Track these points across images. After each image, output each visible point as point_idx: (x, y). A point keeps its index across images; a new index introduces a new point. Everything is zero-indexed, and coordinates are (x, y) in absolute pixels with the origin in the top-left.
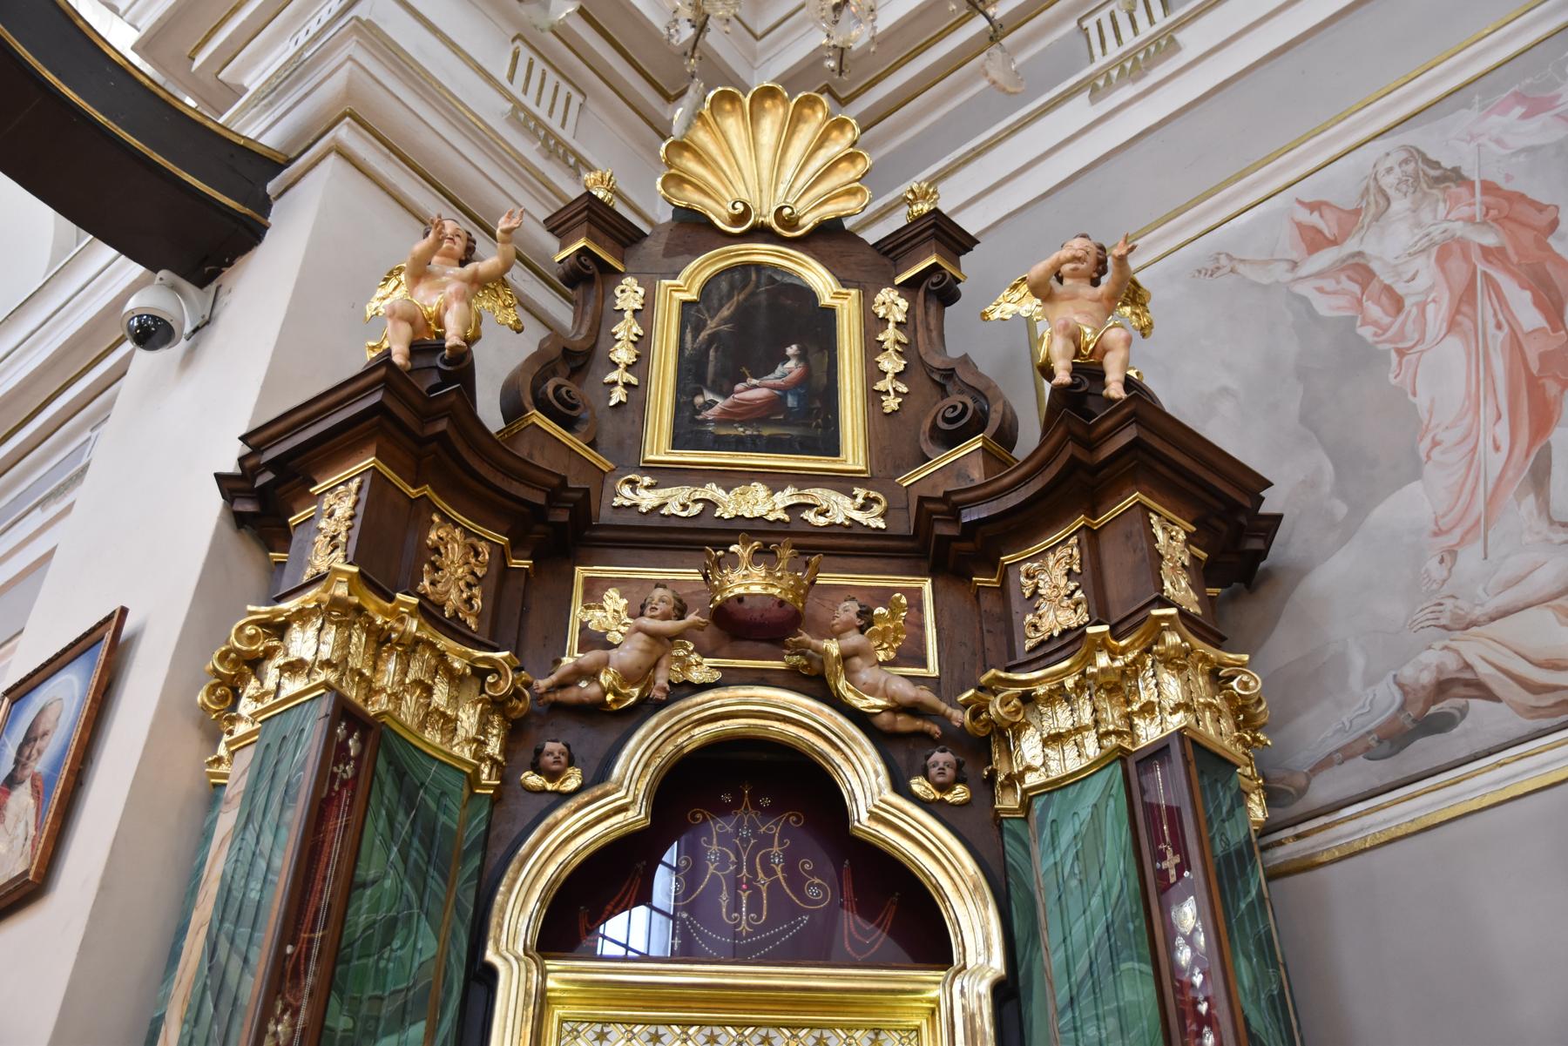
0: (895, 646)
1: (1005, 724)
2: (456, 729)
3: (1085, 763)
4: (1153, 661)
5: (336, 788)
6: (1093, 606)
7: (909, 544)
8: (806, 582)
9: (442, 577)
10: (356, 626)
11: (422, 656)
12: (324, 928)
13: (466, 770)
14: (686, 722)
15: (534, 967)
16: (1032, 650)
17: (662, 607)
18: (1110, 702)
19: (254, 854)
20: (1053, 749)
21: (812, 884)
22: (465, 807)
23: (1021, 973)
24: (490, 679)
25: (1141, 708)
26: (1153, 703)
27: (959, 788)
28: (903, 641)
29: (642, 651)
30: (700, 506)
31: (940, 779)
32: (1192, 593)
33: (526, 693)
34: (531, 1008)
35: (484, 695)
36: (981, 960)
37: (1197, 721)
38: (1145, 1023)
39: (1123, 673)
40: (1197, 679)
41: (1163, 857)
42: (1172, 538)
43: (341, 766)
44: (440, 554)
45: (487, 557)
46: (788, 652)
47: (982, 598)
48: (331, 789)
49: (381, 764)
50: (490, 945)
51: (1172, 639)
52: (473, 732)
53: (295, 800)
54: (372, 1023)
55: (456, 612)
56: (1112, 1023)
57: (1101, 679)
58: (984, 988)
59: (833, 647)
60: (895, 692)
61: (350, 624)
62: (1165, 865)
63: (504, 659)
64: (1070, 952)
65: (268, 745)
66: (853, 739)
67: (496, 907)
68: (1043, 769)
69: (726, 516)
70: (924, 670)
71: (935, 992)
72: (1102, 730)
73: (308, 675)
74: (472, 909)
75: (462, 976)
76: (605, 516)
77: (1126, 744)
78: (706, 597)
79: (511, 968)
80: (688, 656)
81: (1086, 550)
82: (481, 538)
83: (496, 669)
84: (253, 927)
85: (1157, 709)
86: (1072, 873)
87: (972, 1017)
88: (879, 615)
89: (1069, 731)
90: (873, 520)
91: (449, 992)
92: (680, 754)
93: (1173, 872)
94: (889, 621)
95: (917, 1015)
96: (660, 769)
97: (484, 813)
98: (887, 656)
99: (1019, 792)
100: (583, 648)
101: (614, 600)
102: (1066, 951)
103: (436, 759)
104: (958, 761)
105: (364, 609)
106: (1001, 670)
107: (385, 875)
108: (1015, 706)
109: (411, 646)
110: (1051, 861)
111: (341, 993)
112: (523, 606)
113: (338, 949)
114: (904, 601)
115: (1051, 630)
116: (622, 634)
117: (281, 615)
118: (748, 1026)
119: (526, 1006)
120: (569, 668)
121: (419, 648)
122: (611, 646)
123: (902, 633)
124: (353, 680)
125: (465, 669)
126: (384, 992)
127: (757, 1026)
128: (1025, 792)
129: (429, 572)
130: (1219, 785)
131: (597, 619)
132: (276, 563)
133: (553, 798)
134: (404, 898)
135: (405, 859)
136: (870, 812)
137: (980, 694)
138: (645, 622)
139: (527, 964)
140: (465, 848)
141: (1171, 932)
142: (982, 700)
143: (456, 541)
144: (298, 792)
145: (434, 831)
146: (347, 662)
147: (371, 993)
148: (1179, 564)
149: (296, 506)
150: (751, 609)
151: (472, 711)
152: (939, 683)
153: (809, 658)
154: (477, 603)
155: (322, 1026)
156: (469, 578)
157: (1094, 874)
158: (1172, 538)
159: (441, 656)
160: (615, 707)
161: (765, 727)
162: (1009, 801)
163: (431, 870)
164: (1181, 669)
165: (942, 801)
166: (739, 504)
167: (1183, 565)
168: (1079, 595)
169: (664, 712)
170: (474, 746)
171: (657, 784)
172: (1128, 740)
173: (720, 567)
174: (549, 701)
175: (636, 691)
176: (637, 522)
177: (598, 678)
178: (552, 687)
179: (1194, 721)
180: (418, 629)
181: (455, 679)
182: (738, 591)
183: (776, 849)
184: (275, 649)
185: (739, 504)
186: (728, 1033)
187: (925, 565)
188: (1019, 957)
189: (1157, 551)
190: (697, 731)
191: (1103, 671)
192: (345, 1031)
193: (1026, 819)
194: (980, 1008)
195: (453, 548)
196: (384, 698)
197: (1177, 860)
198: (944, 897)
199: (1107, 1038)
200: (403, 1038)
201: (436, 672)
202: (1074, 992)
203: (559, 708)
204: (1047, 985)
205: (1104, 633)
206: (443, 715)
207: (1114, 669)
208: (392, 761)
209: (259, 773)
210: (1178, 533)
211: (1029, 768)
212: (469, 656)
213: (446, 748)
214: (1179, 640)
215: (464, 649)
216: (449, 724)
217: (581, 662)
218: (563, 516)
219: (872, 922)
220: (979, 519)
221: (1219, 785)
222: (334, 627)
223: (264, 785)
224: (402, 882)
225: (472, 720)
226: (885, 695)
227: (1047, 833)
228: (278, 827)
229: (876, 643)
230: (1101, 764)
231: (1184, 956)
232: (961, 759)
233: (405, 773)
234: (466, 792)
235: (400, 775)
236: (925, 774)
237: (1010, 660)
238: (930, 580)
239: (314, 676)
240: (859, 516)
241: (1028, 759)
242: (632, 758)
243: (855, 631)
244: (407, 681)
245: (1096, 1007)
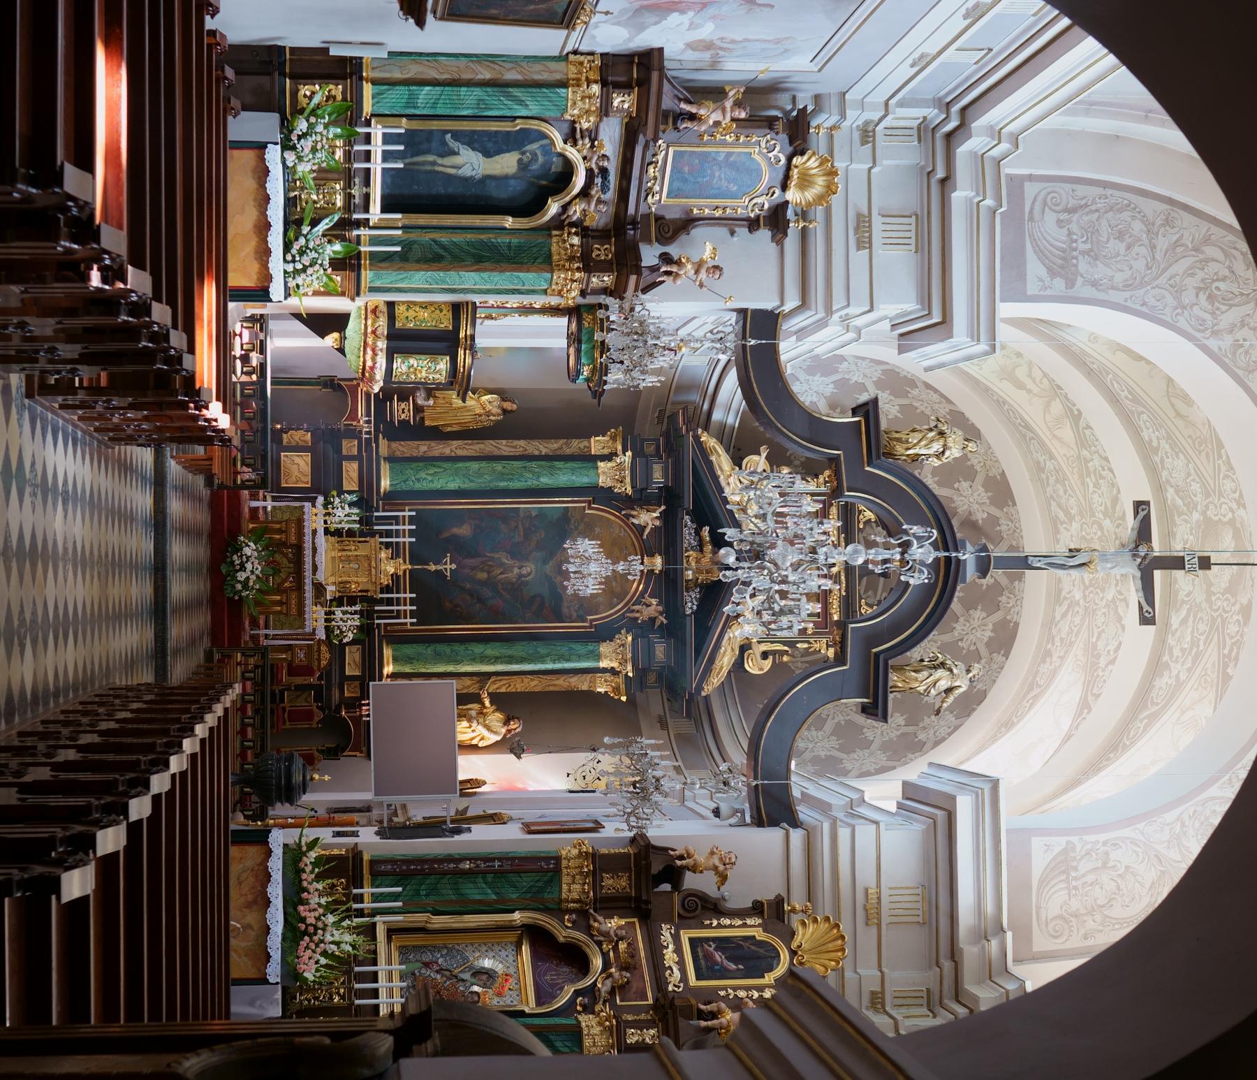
235: (550, 881)
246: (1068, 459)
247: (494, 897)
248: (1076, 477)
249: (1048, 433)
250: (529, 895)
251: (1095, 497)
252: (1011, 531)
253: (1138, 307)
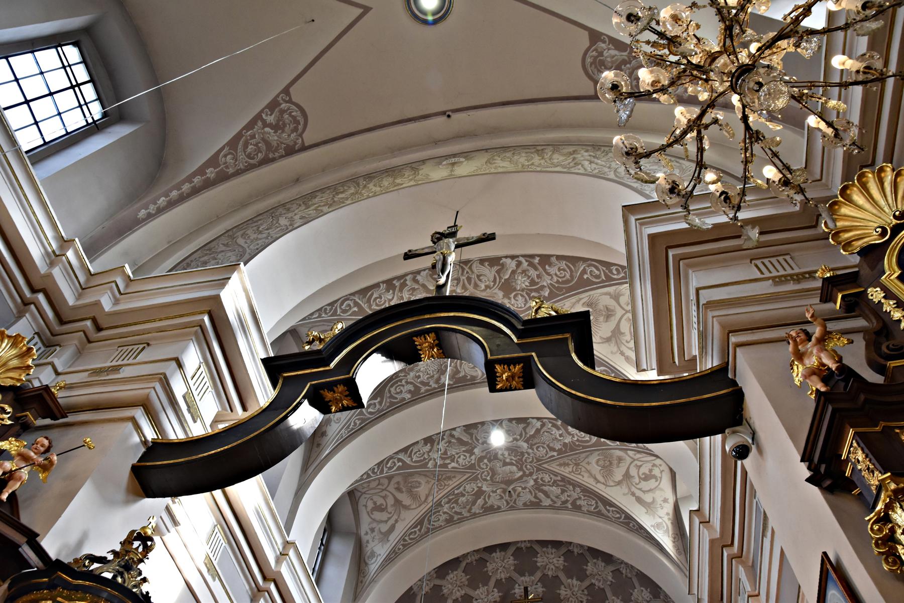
246: (440, 489)
248: (451, 482)
249: (423, 506)
251: (461, 460)
252: (504, 570)
253: (257, 251)
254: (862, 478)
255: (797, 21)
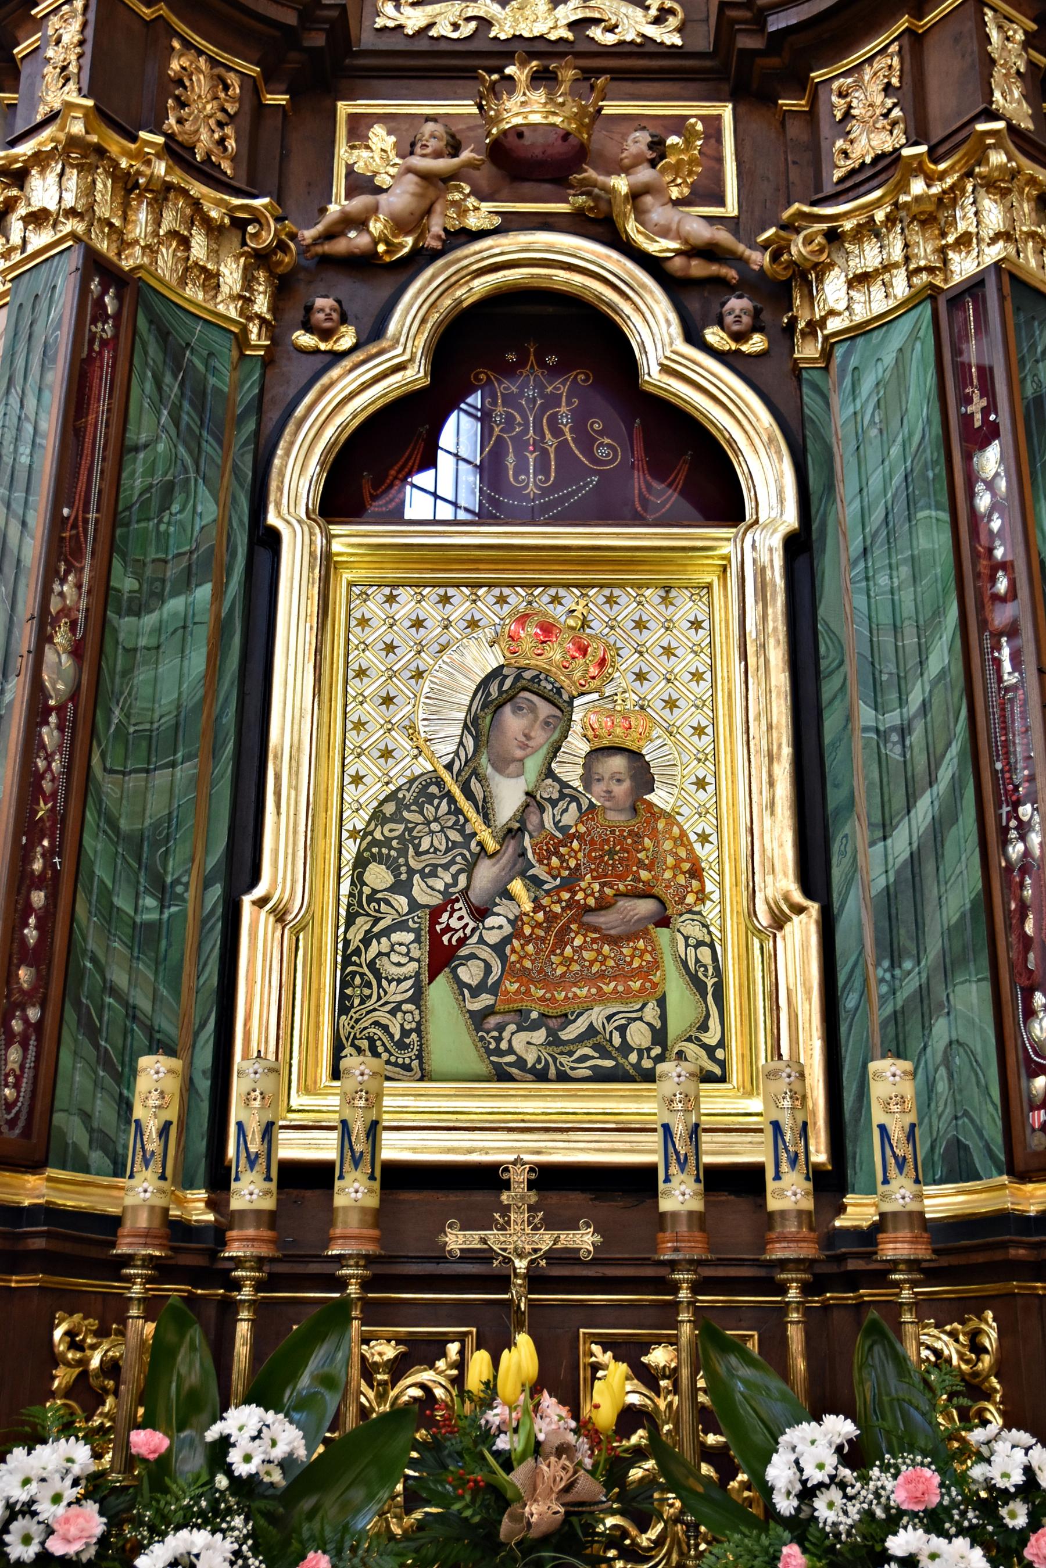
0: (689, 180)
1: (808, 265)
2: (219, 286)
3: (892, 303)
4: (974, 186)
5: (96, 347)
6: (911, 124)
7: (708, 63)
8: (591, 109)
9: (190, 114)
10: (100, 171)
11: (175, 204)
12: (98, 511)
13: (233, 329)
14: (464, 272)
15: (317, 531)
16: (841, 180)
17: (433, 144)
18: (923, 235)
19: (19, 418)
20: (859, 291)
21: (601, 444)
22: (235, 369)
23: (815, 527)
24: (251, 229)
25: (957, 239)
26: (970, 233)
27: (757, 337)
28: (698, 174)
29: (414, 194)
30: (473, 25)
31: (736, 328)
32: (1025, 105)
33: (292, 245)
34: (317, 570)
35: (246, 248)
36: (773, 514)
37: (1018, 252)
38: (939, 570)
39: (940, 200)
40: (1021, 206)
41: (968, 400)
42: (1008, 39)
43: (100, 325)
44: (185, 88)
45: (238, 91)
46: (572, 192)
47: (789, 123)
48: (91, 349)
49: (142, 323)
50: (271, 508)
51: (997, 158)
52: (237, 289)
53: (54, 361)
54: (158, 584)
55: (208, 155)
56: (905, 571)
57: (915, 209)
58: (776, 541)
59: (621, 184)
60: (689, 233)
61: (92, 169)
62: (970, 409)
63: (265, 207)
64: (866, 503)
65: (21, 305)
66: (643, 286)
67: (275, 472)
68: (847, 313)
69: (503, 36)
70: (722, 210)
71: (727, 548)
72: (912, 267)
73: (54, 226)
74: (250, 474)
75: (246, 540)
76: (367, 41)
77: (938, 281)
78: (481, 132)
79: (294, 531)
80: (464, 200)
81: (907, 58)
82: (230, 69)
83: (256, 218)
84: (28, 491)
85: (975, 240)
86: (872, 422)
87: (763, 569)
88: (672, 146)
89: (876, 270)
90: (668, 36)
91: (233, 555)
92: (459, 309)
93: (978, 416)
94: (682, 151)
95: (708, 572)
96: (438, 324)
97: (256, 376)
98: (681, 193)
99: (820, 340)
100: (348, 197)
101: (380, 137)
102: (862, 501)
103: (200, 318)
104: (755, 308)
105: (106, 151)
106: (805, 204)
107: (157, 439)
108: (819, 244)
109: (161, 194)
110: (851, 410)
111: (124, 556)
112: (282, 147)
113: (116, 513)
114: (700, 127)
115: (863, 156)
116: (392, 177)
117: (17, 161)
118: (537, 587)
119: (311, 568)
120: (336, 216)
121: (172, 195)
122: (380, 190)
123: (698, 165)
124: (103, 232)
125: (222, 219)
126: (167, 554)
127: (547, 586)
128: (826, 338)
129: (174, 108)
130: (1036, 324)
131: (363, 160)
132: (8, 105)
133: (328, 358)
134: (179, 462)
135: (177, 423)
136: (661, 364)
137: (782, 233)
138: (416, 161)
139: (310, 528)
140: (239, 412)
141: (971, 479)
142: (783, 239)
143: (201, 72)
144: (56, 353)
145: (204, 393)
146: (94, 211)
147: (154, 556)
148: (1013, 71)
149: (20, 34)
150: (533, 145)
151: (234, 266)
152: (738, 224)
153: (596, 199)
154: (231, 144)
155: (108, 587)
156: (220, 116)
157: (895, 423)
158: (1008, 39)
159: (196, 204)
160: (387, 259)
161: (549, 277)
162: (809, 350)
163: (205, 434)
164: (1005, 193)
165: (738, 351)
166: (516, 21)
167: (1018, 72)
168: (896, 113)
169: (440, 263)
170: (240, 303)
171: (435, 340)
172: (941, 276)
173: (495, 94)
174: (317, 255)
175: (409, 241)
176: (402, 45)
177: (367, 226)
178: (319, 237)
179: (1014, 252)
180: (167, 173)
181: (213, 230)
182: (518, 120)
183: (564, 409)
184: (16, 199)
185: (516, 21)
186: (518, 593)
187: (726, 88)
188: (813, 510)
189: (989, 54)
190: (476, 283)
191: (918, 199)
192: (130, 592)
193: (826, 369)
194: (771, 561)
195: (199, 80)
196: (138, 251)
197: (984, 403)
198: (738, 452)
199: (899, 587)
200: (191, 599)
201: (193, 224)
202: (869, 542)
203: (327, 261)
204: (841, 538)
205: (921, 154)
206: (204, 269)
207: (929, 197)
208: (153, 320)
209: (15, 335)
210: (1015, 32)
211: (832, 313)
212: (226, 204)
213: (210, 306)
214: (1004, 159)
215: (219, 195)
216: (211, 280)
217: (348, 209)
218: (318, 40)
219: (662, 481)
220: (788, 27)
221: (1036, 324)
222: (75, 171)
223: (22, 347)
224: (175, 446)
225: (235, 275)
226: (678, 236)
227: (848, 381)
228: (40, 390)
229: (668, 178)
230: (910, 304)
231: (984, 502)
232: (759, 306)
233: (169, 333)
234: (235, 354)
235: (164, 335)
236: (721, 323)
237: (816, 193)
238: (730, 106)
239: (60, 227)
240: (654, 32)
241: (832, 304)
242: (408, 313)
243: (646, 165)
244: (162, 233)
245: (890, 557)
247: (204, 592)
250: (210, 447)
254: (39, 78)
255: (476, 466)
